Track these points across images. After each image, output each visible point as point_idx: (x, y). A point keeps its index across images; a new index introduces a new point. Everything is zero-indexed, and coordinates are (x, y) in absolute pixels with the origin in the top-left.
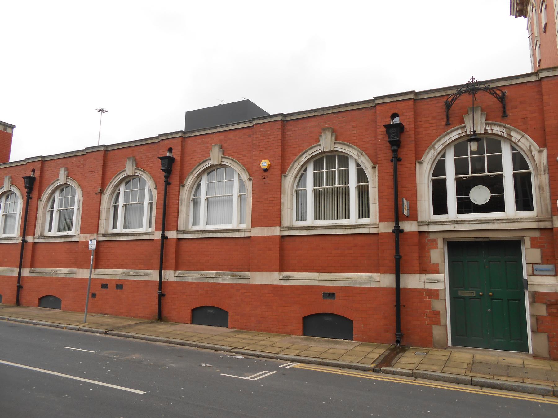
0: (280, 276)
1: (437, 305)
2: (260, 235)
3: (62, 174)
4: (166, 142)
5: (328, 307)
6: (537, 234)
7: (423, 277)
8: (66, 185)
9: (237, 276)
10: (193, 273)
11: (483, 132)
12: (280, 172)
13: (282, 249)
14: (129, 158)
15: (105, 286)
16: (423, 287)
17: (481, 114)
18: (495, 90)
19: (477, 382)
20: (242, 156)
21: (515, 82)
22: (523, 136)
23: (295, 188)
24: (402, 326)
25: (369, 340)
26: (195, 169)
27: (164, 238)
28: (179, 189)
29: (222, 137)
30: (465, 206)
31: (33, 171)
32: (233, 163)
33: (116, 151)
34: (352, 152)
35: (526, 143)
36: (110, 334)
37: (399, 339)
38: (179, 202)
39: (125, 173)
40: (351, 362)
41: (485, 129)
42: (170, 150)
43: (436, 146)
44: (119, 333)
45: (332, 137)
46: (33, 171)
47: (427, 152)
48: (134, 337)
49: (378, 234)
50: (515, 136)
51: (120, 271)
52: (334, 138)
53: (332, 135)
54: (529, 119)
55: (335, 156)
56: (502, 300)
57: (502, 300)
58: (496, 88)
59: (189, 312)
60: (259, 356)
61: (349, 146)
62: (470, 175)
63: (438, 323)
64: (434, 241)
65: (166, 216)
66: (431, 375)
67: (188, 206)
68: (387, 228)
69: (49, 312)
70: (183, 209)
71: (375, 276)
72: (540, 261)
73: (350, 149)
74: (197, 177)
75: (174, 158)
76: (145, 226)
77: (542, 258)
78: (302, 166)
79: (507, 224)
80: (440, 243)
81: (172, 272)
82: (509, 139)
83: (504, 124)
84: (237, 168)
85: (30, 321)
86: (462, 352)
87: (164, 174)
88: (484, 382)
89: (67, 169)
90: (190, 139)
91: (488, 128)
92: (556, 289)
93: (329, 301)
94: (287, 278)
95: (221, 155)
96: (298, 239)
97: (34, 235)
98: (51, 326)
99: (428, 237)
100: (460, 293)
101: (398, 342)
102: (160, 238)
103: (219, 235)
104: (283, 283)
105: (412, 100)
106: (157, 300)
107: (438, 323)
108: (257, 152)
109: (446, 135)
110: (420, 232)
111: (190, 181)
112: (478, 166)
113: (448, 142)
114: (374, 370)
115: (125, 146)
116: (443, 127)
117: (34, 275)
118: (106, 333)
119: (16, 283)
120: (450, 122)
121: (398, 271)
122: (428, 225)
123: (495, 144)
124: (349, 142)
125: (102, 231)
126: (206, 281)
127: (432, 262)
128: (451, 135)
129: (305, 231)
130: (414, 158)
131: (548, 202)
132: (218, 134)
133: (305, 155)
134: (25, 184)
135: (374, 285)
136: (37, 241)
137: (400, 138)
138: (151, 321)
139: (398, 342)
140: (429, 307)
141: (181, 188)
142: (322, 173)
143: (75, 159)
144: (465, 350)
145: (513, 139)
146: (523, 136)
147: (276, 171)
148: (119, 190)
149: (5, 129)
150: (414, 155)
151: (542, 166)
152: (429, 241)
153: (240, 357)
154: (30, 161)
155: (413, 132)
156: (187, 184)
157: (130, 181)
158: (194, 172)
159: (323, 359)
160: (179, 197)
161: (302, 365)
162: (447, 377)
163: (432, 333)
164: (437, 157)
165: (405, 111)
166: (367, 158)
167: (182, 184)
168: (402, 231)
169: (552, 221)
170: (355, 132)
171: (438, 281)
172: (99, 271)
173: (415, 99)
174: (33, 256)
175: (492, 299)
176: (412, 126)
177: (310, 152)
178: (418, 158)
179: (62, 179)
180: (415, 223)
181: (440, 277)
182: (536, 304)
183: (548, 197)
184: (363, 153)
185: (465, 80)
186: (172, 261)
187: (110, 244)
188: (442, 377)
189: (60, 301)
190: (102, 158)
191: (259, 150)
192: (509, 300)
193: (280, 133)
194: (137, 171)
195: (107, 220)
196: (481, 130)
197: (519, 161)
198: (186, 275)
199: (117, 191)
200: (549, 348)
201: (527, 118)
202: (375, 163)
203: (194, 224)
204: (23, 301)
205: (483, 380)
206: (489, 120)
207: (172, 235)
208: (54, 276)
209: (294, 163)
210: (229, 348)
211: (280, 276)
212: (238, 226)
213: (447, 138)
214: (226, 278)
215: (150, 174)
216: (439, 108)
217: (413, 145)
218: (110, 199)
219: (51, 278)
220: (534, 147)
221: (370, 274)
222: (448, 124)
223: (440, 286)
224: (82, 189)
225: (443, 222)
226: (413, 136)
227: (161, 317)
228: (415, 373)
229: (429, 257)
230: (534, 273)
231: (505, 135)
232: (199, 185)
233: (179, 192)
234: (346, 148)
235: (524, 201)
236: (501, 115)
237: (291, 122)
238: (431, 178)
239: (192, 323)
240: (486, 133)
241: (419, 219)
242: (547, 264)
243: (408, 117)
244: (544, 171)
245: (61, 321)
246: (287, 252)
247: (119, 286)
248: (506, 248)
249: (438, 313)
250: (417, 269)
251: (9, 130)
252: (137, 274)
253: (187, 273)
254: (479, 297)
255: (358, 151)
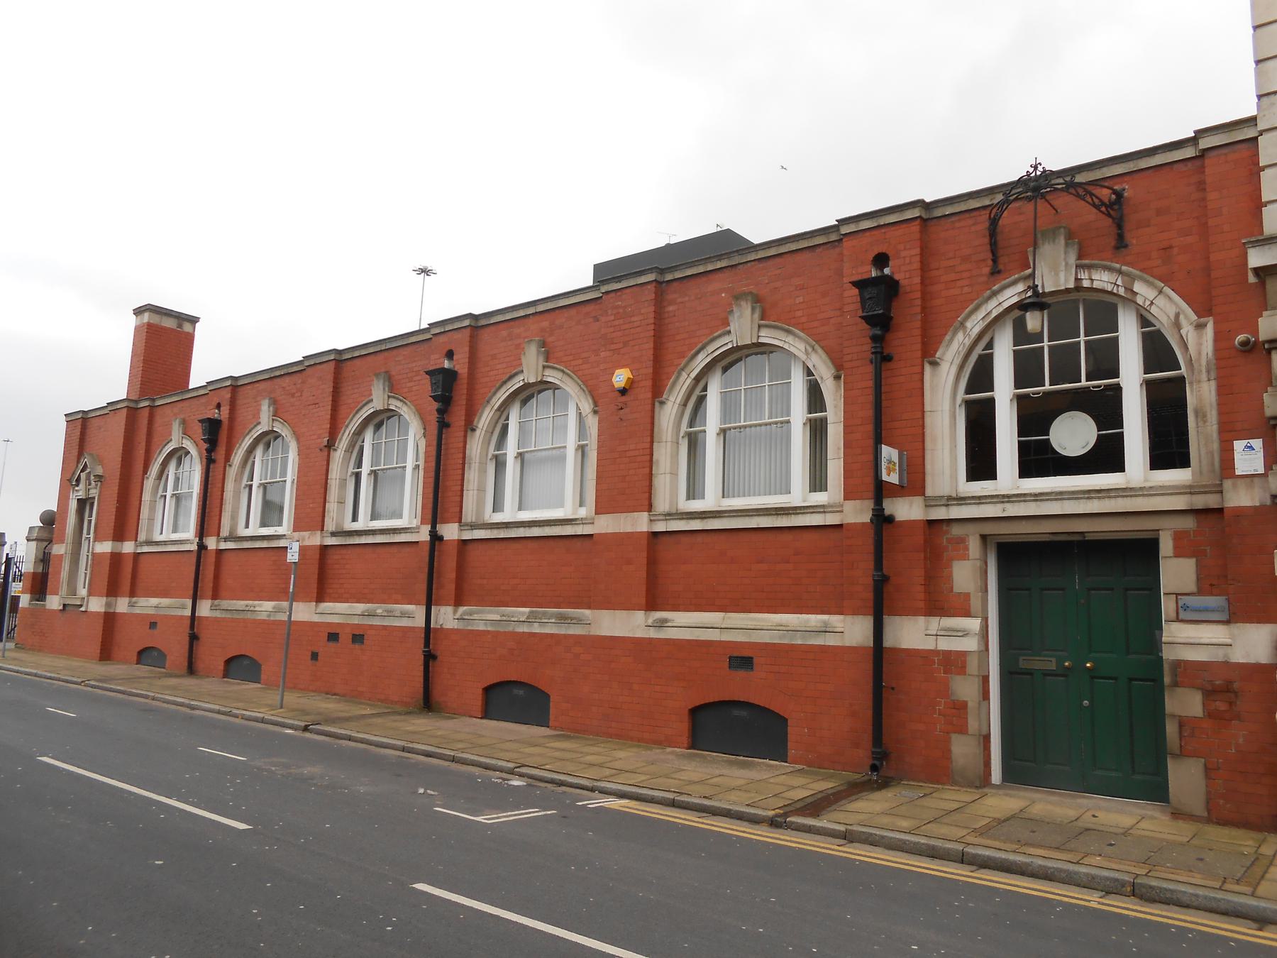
0: (646, 620)
1: (964, 689)
2: (610, 530)
3: (265, 410)
4: (442, 339)
5: (750, 688)
6: (1189, 523)
7: (935, 623)
8: (388, 413)
9: (566, 619)
10: (489, 612)
11: (1071, 285)
12: (649, 395)
13: (652, 562)
14: (377, 375)
15: (333, 637)
16: (932, 647)
17: (1067, 245)
18: (1090, 188)
19: (975, 856)
20: (580, 361)
21: (1144, 163)
22: (1160, 292)
23: (684, 428)
24: (887, 730)
25: (816, 763)
26: (495, 393)
27: (436, 538)
28: (465, 437)
29: (545, 324)
30: (1037, 459)
31: (218, 406)
32: (565, 378)
33: (357, 362)
34: (795, 345)
35: (1166, 307)
36: (311, 731)
37: (877, 763)
38: (464, 464)
39: (370, 405)
40: (734, 803)
41: (1077, 279)
42: (450, 355)
43: (969, 325)
44: (332, 730)
45: (753, 313)
46: (450, 355)
47: (947, 338)
48: (350, 739)
49: (840, 526)
50: (1144, 291)
51: (360, 607)
52: (757, 315)
53: (753, 309)
54: (1175, 250)
55: (1076, 302)
56: (1115, 679)
57: (1115, 679)
58: (1094, 183)
59: (480, 691)
60: (561, 784)
61: (788, 332)
62: (1047, 387)
63: (963, 730)
64: (962, 541)
65: (441, 496)
66: (883, 837)
67: (483, 471)
68: (858, 513)
69: (236, 688)
70: (471, 477)
71: (836, 620)
72: (1192, 587)
73: (790, 339)
74: (498, 409)
75: (897, 282)
76: (407, 515)
77: (1198, 579)
78: (697, 379)
79: (1120, 500)
80: (974, 546)
81: (449, 609)
82: (1130, 299)
83: (1118, 266)
84: (570, 387)
85: (187, 701)
86: (1011, 796)
87: (436, 405)
88: (989, 858)
89: (274, 402)
90: (487, 330)
91: (1083, 275)
92: (1225, 655)
93: (741, 673)
94: (661, 624)
95: (541, 362)
96: (685, 540)
97: (218, 535)
98: (219, 712)
99: (947, 532)
100: (1023, 664)
101: (874, 768)
102: (428, 538)
103: (536, 532)
104: (653, 634)
105: (918, 222)
106: (422, 668)
107: (963, 730)
108: (608, 353)
109: (989, 298)
110: (931, 523)
111: (485, 418)
112: (1065, 365)
113: (994, 314)
114: (774, 823)
115: (371, 350)
116: (985, 279)
117: (218, 614)
118: (306, 729)
119: (188, 630)
120: (1001, 267)
121: (880, 608)
122: (947, 505)
123: (1103, 313)
124: (788, 322)
125: (330, 525)
126: (510, 629)
127: (956, 590)
128: (1001, 298)
129: (698, 521)
130: (919, 354)
131: (1216, 446)
132: (537, 317)
133: (701, 356)
134: (434, 390)
135: (831, 641)
136: (223, 546)
137: (888, 309)
138: (398, 708)
139: (874, 768)
140: (945, 691)
141: (469, 433)
142: (1042, 348)
143: (287, 379)
144: (1021, 793)
145: (1140, 300)
146: (1160, 292)
147: (644, 393)
148: (507, 419)
149: (180, 326)
150: (919, 346)
151: (1204, 363)
152: (949, 541)
153: (516, 782)
154: (214, 387)
155: (918, 295)
156: (480, 426)
157: (531, 396)
158: (494, 400)
159: (681, 793)
160: (464, 453)
161: (633, 804)
162: (915, 843)
163: (949, 751)
164: (975, 348)
165: (901, 247)
166: (824, 356)
167: (470, 427)
168: (890, 520)
169: (1222, 492)
170: (801, 299)
171: (965, 634)
172: (327, 606)
173: (925, 218)
174: (217, 577)
175: (1092, 678)
176: (917, 280)
177: (710, 348)
178: (928, 353)
179: (531, 367)
180: (918, 501)
181: (974, 624)
182: (1179, 690)
183: (1215, 435)
184: (817, 347)
185: (1012, 171)
186: (450, 588)
187: (344, 551)
188: (904, 842)
189: (260, 665)
190: (330, 377)
191: (613, 347)
192: (1131, 680)
193: (652, 309)
194: (392, 401)
195: (341, 502)
196: (1066, 280)
197: (1157, 351)
198: (476, 617)
199: (359, 443)
200: (1208, 793)
201: (1171, 247)
202: (840, 368)
203: (691, 495)
204: (200, 666)
205: (987, 853)
206: (1086, 256)
207: (450, 532)
208: (249, 616)
209: (679, 375)
210: (511, 765)
211: (646, 620)
212: (575, 512)
213: (992, 304)
214: (546, 623)
215: (415, 406)
216: (973, 236)
217: (918, 324)
218: (346, 460)
219: (245, 621)
220: (1186, 317)
221: (825, 617)
222: (996, 272)
223: (970, 644)
224: (298, 440)
225: (980, 498)
226: (919, 302)
227: (428, 704)
228: (851, 832)
229: (950, 578)
230: (1181, 617)
231: (1122, 291)
232: (702, 399)
233: (465, 443)
234: (782, 335)
235: (1169, 448)
236: (1113, 243)
237: (675, 284)
238: (961, 395)
239: (486, 715)
240: (1078, 288)
241: (929, 492)
242: (1212, 594)
243: (907, 260)
244: (1208, 372)
245: (240, 705)
246: (661, 568)
247: (358, 638)
248: (1123, 557)
249: (962, 707)
250: (922, 604)
251: (187, 327)
252: (389, 614)
253: (477, 613)
254: (1065, 673)
255: (807, 343)
